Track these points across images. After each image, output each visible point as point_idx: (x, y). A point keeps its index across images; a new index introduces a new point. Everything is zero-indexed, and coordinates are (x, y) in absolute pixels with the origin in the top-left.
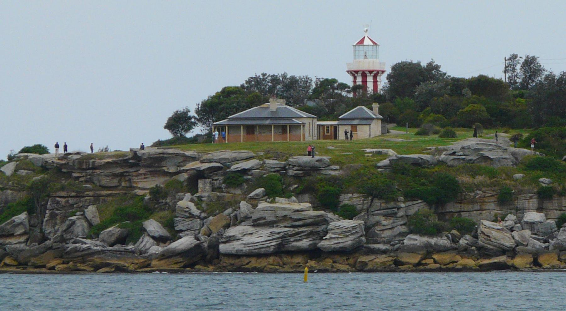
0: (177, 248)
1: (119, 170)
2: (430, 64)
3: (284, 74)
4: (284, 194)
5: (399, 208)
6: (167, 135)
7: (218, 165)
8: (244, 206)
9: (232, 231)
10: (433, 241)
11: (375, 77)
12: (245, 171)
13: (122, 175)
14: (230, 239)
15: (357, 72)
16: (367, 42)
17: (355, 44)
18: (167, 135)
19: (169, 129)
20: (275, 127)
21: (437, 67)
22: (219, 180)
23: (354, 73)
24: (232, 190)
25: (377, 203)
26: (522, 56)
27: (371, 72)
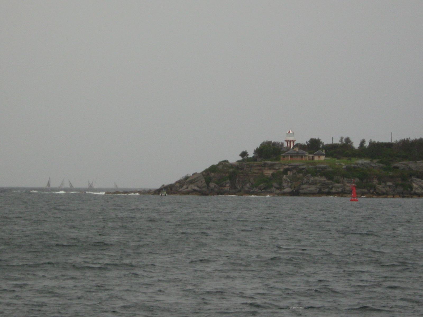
0: (417, 197)
1: (259, 168)
2: (318, 139)
3: (342, 137)
4: (317, 176)
5: (352, 180)
6: (240, 158)
7: (294, 167)
8: (305, 179)
9: (304, 186)
10: (363, 190)
11: (293, 143)
12: (303, 169)
13: (260, 169)
14: (303, 189)
15: (288, 141)
16: (291, 132)
17: (287, 132)
18: (240, 158)
19: (241, 156)
20: (286, 156)
21: (320, 140)
22: (295, 171)
23: (287, 141)
24: (299, 174)
25: (345, 179)
26: (345, 137)
27: (292, 141)
